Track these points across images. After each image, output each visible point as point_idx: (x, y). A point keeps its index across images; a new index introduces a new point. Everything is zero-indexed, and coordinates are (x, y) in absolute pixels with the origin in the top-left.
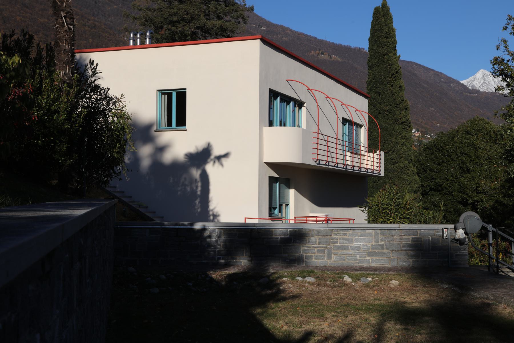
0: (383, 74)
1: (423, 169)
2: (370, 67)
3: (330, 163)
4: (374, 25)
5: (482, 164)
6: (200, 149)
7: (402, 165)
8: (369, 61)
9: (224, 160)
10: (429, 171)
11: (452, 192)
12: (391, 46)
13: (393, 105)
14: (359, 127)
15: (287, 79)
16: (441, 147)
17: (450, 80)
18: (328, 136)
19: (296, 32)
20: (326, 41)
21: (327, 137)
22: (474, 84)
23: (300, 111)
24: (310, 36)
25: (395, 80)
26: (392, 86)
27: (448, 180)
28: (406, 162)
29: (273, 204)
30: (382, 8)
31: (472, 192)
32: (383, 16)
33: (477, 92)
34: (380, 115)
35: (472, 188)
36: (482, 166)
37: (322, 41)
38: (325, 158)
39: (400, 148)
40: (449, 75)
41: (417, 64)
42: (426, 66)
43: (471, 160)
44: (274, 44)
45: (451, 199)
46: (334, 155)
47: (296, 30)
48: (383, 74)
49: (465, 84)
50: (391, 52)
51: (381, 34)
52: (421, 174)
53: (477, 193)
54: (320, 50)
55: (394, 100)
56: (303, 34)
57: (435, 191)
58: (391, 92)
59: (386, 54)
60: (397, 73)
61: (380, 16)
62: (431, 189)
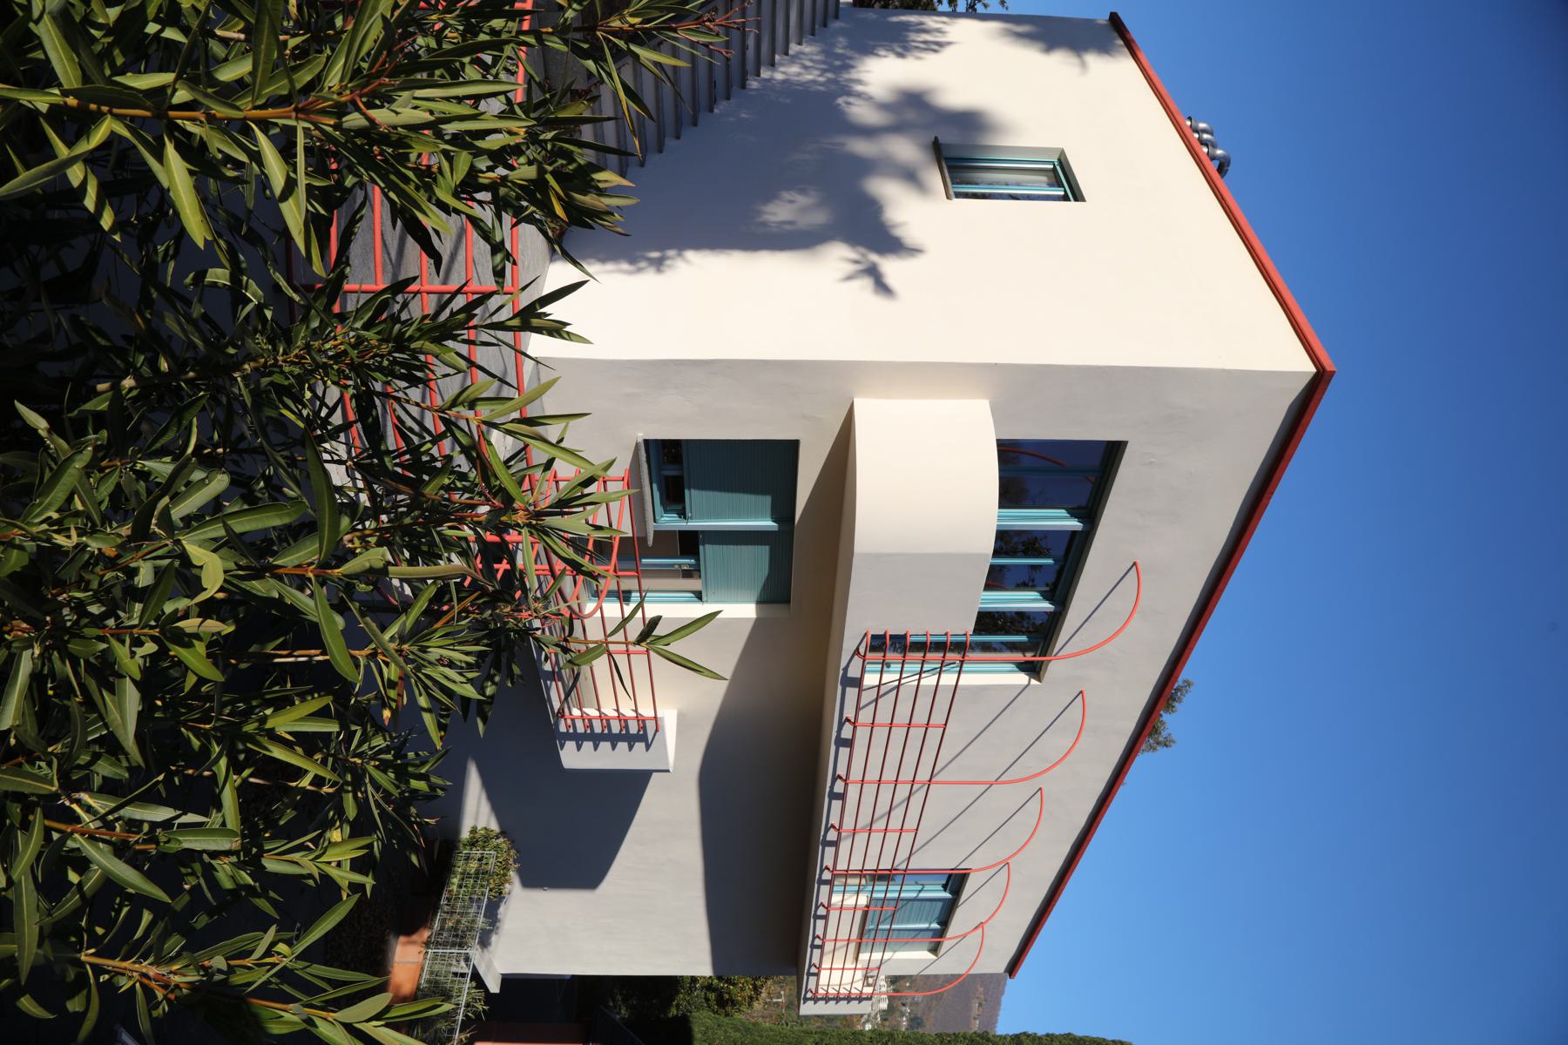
3: (816, 978)
6: (898, 232)
9: (867, 283)
15: (1085, 693)
18: (917, 830)
20: (999, 1010)
21: (944, 723)
23: (1012, 667)
29: (711, 546)
37: (999, 1003)
38: (831, 934)
54: (986, 1000)
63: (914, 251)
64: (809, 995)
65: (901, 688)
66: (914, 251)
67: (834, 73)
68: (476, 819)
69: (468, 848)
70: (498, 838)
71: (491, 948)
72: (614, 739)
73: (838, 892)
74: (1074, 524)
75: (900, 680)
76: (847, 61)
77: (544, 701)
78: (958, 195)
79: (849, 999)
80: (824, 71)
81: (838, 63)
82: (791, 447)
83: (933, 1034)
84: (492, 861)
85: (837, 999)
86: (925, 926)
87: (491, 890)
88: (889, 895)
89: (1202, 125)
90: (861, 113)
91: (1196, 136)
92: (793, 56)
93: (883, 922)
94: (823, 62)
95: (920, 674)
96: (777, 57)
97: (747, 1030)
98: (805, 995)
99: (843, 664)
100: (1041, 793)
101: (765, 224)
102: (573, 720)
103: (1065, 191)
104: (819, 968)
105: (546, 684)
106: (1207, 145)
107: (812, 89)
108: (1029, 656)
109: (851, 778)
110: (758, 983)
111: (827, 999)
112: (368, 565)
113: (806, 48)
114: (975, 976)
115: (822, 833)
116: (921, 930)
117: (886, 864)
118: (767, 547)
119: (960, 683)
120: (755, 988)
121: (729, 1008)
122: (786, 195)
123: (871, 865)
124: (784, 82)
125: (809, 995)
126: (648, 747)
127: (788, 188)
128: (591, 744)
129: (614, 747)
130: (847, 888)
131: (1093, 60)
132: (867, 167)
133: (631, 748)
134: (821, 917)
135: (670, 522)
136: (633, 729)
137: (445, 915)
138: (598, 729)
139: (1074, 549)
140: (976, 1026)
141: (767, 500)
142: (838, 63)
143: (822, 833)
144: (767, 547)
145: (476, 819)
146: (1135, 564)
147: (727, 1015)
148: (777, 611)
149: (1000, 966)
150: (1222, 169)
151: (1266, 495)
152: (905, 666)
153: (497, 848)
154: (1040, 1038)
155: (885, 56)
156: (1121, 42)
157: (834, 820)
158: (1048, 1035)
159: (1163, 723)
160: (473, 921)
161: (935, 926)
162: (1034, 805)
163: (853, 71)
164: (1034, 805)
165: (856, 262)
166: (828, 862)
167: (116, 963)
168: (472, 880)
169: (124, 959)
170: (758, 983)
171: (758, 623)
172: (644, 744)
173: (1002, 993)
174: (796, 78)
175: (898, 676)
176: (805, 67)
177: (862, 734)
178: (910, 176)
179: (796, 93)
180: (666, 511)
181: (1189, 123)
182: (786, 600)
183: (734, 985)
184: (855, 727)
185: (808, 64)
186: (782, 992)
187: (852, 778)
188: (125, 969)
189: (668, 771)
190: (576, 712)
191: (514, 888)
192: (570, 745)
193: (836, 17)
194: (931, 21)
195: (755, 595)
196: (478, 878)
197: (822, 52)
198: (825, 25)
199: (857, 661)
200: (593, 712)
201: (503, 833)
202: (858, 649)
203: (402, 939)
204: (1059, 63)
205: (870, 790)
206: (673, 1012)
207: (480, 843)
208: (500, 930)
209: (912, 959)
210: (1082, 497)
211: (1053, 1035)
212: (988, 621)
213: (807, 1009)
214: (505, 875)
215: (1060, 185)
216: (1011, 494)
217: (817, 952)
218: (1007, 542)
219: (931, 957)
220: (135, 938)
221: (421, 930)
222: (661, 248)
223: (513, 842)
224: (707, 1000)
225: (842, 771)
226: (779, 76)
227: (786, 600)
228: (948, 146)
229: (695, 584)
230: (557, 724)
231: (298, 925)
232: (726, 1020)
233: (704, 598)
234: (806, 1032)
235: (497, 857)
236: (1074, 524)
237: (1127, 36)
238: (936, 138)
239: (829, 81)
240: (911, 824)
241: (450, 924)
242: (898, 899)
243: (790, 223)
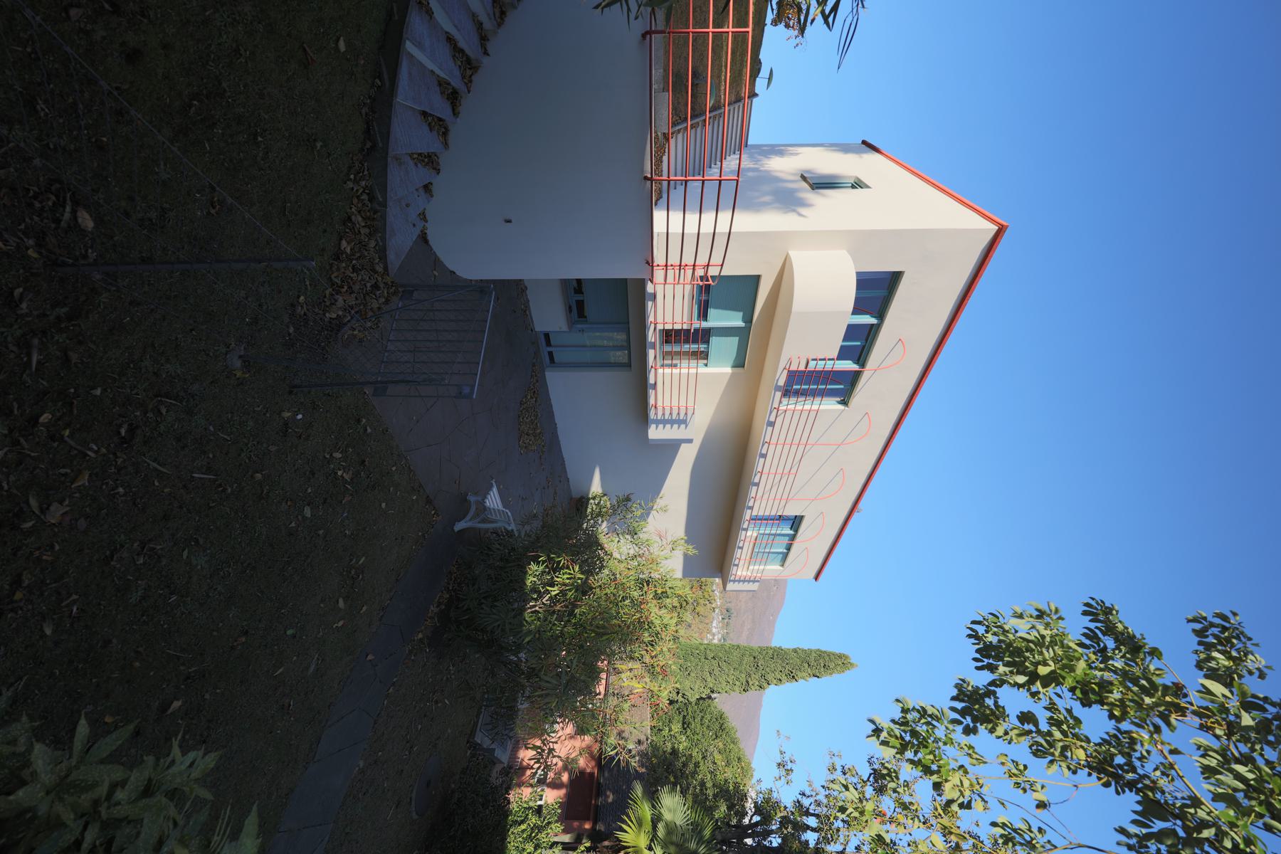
2: (795, 651)
23: (835, 402)
28: (711, 685)
44: (977, 278)
57: (683, 721)
58: (775, 670)
59: (809, 665)
74: (873, 321)
82: (757, 278)
100: (808, 551)
118: (738, 338)
141: (740, 314)
144: (738, 338)
171: (733, 374)
177: (742, 562)
195: (731, 362)
219: (781, 568)
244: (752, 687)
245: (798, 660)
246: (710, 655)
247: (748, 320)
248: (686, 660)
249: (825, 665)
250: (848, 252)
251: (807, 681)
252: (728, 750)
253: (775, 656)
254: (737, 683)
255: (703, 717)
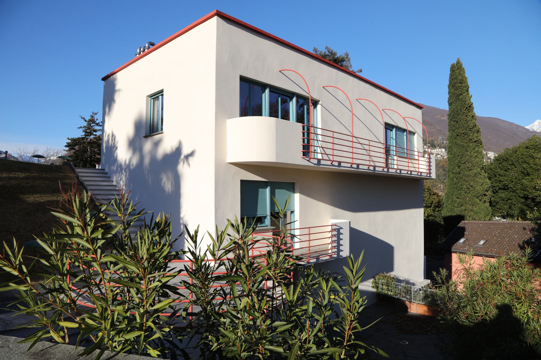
0: (459, 108)
1: (494, 174)
4: (451, 76)
5: (538, 169)
6: (174, 149)
7: (475, 171)
8: (449, 100)
9: (191, 159)
10: (498, 176)
11: (516, 190)
12: (464, 89)
13: (468, 129)
14: (412, 134)
15: (324, 86)
16: (507, 159)
17: (518, 127)
19: (427, 106)
22: (533, 128)
23: (315, 110)
24: (436, 108)
25: (469, 112)
26: (466, 116)
27: (513, 182)
28: (479, 169)
30: (457, 64)
31: (532, 190)
32: (458, 69)
33: (536, 132)
34: (458, 137)
35: (531, 186)
36: (538, 171)
39: (474, 159)
40: (518, 124)
41: (498, 119)
42: (504, 119)
43: (530, 167)
45: (515, 196)
46: (417, 166)
47: (428, 105)
48: (459, 108)
49: (528, 128)
50: (464, 93)
51: (456, 81)
52: (492, 178)
53: (536, 190)
55: (468, 125)
56: (432, 107)
57: (503, 189)
58: (466, 120)
59: (461, 94)
60: (470, 107)
61: (455, 69)
62: (500, 189)
63: (180, 144)
64: (428, 175)
65: (323, 147)
66: (180, 144)
67: (122, 170)
68: (369, 286)
69: (379, 289)
70: (376, 279)
71: (415, 282)
72: (339, 239)
73: (393, 166)
74: (267, 91)
75: (320, 147)
76: (119, 165)
77: (327, 262)
78: (162, 129)
79: (430, 162)
80: (122, 173)
81: (119, 169)
82: (243, 182)
83: (449, 133)
84: (383, 281)
85: (430, 166)
86: (405, 137)
87: (393, 281)
88: (394, 150)
89: (138, 51)
90: (135, 161)
91: (142, 53)
92: (117, 184)
93: (404, 151)
94: (119, 173)
95: (318, 141)
96: (117, 189)
97: (448, 197)
98: (409, 174)
99: (313, 165)
101: (172, 192)
102: (332, 253)
103: (160, 95)
104: (419, 172)
105: (320, 261)
106: (145, 49)
107: (128, 177)
108: (311, 104)
109: (368, 164)
110: (432, 193)
111: (430, 170)
112: (245, 268)
113: (114, 179)
114: (423, 121)
115: (371, 171)
116: (407, 138)
117: (383, 151)
119: (321, 128)
120: (434, 194)
121: (441, 204)
122: (163, 184)
123: (383, 156)
124: (126, 186)
125: (428, 175)
126: (342, 228)
127: (161, 184)
128: (341, 247)
129: (342, 239)
130: (392, 163)
131: (118, 87)
132: (153, 159)
133: (342, 234)
134: (400, 172)
135: (268, 221)
136: (335, 233)
137: (401, 296)
138: (336, 244)
139: (275, 91)
140: (446, 118)
141: (260, 190)
142: (119, 169)
143: (371, 171)
145: (369, 286)
146: (280, 71)
147: (443, 204)
148: (297, 187)
149: (419, 112)
150: (153, 44)
151: (257, 30)
152: (315, 145)
153: (379, 279)
154: (450, 96)
155: (117, 153)
156: (111, 77)
157: (366, 167)
158: (449, 94)
159: (340, 56)
160: (403, 287)
161: (405, 134)
162: (362, 102)
163: (122, 164)
164: (362, 102)
165: (184, 162)
166: (381, 169)
167: (346, 336)
168: (390, 287)
169: (345, 335)
170: (432, 193)
171: (301, 193)
172: (341, 230)
173: (438, 109)
174: (124, 182)
175: (319, 148)
176: (121, 179)
177: (336, 158)
178: (157, 144)
179: (130, 181)
180: (264, 223)
181: (138, 55)
182: (293, 184)
183: (433, 202)
184: (334, 161)
185: (120, 178)
186: (439, 185)
187: (351, 162)
188: (348, 334)
189: (350, 222)
190: (330, 251)
191: (392, 274)
192: (341, 253)
193: (104, 170)
194: (105, 138)
195: (292, 194)
196: (389, 286)
197: (116, 175)
198: (107, 173)
199: (312, 160)
200: (330, 246)
201: (374, 277)
202: (308, 160)
203: (409, 310)
204: (118, 97)
205: (355, 156)
206: (442, 223)
207: (377, 285)
208: (409, 280)
209: (417, 142)
210: (258, 88)
211: (448, 92)
212: (300, 119)
213: (433, 176)
214: (388, 277)
215: (158, 97)
216: (258, 112)
217: (413, 173)
218: (273, 113)
219: (416, 134)
220: (339, 331)
221: (406, 304)
222: (180, 224)
223: (377, 274)
224: (438, 211)
225: (349, 165)
226: (124, 188)
227: (293, 184)
228: (146, 133)
229: (289, 213)
230: (334, 258)
231: (401, 342)
232: (445, 204)
233: (293, 210)
234: (449, 177)
235: (382, 279)
236: (267, 91)
237: (110, 75)
238: (143, 137)
239: (125, 171)
240: (367, 142)
241: (404, 294)
242: (396, 147)
243: (172, 184)
244: (479, 138)
245: (458, 102)
246: (457, 170)
247: (264, 185)
248: (462, 189)
249: (460, 83)
250: (228, 119)
251: (471, 96)
252: (522, 156)
253: (456, 119)
254: (476, 149)
255: (499, 175)
